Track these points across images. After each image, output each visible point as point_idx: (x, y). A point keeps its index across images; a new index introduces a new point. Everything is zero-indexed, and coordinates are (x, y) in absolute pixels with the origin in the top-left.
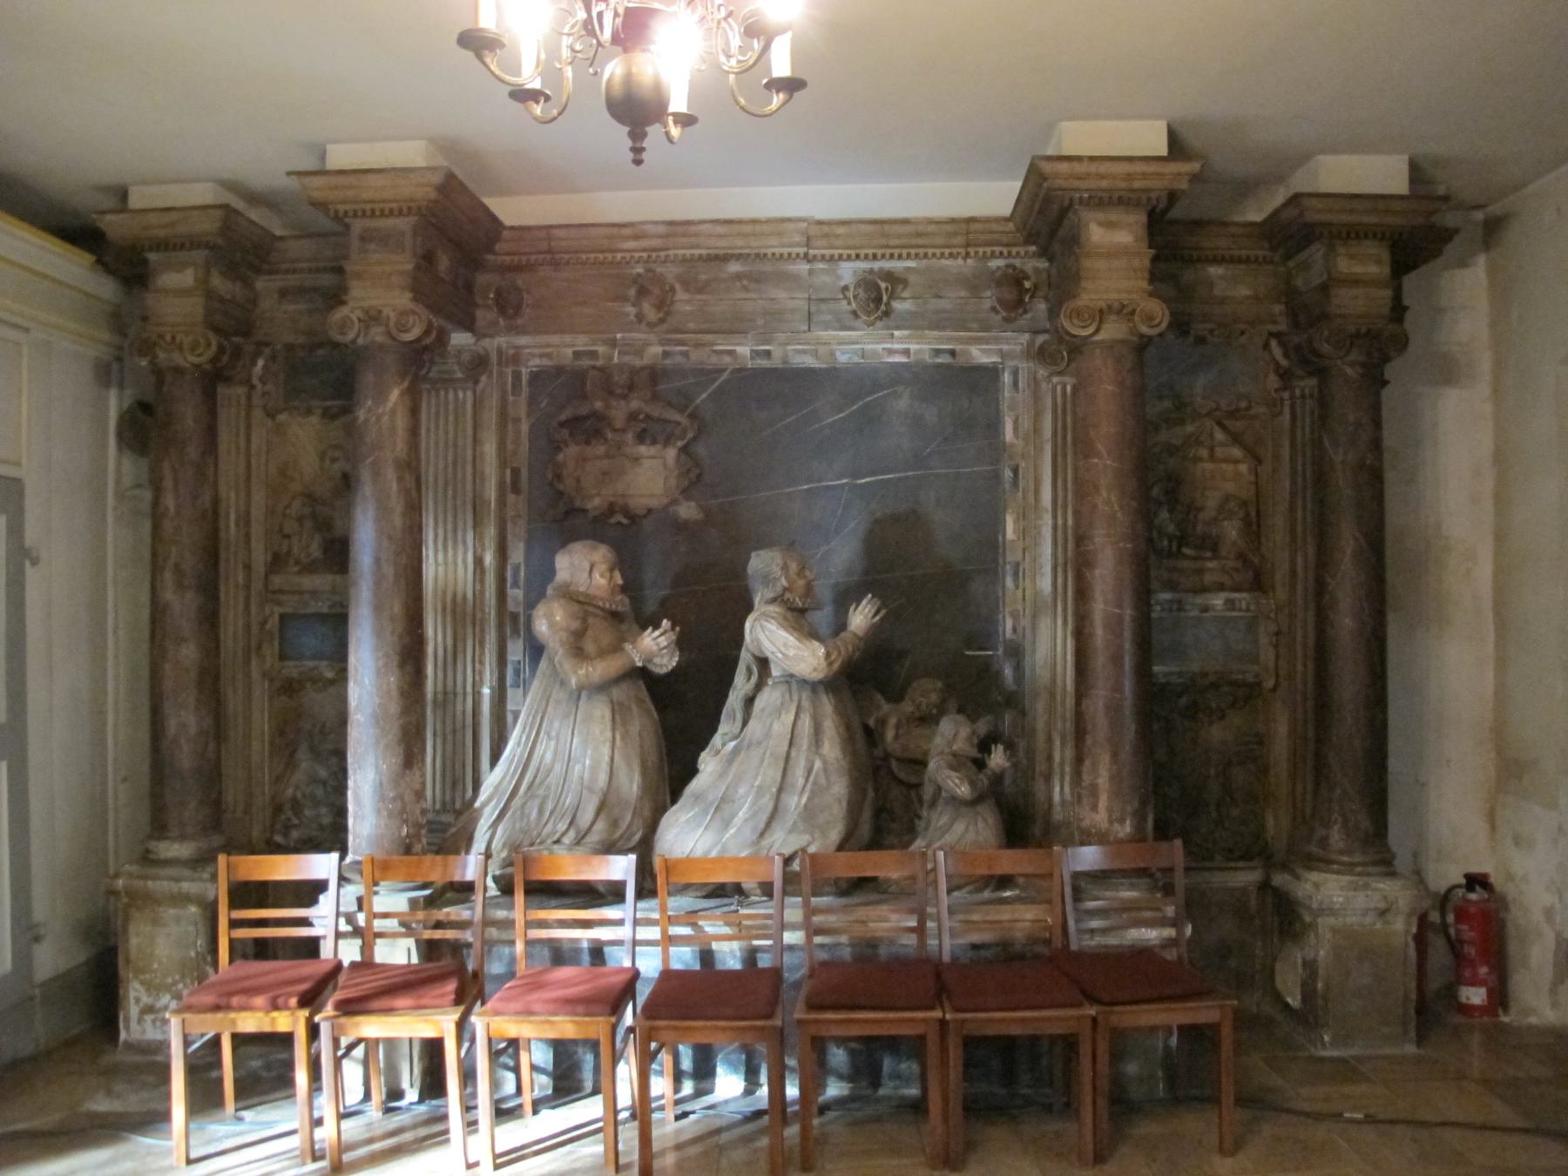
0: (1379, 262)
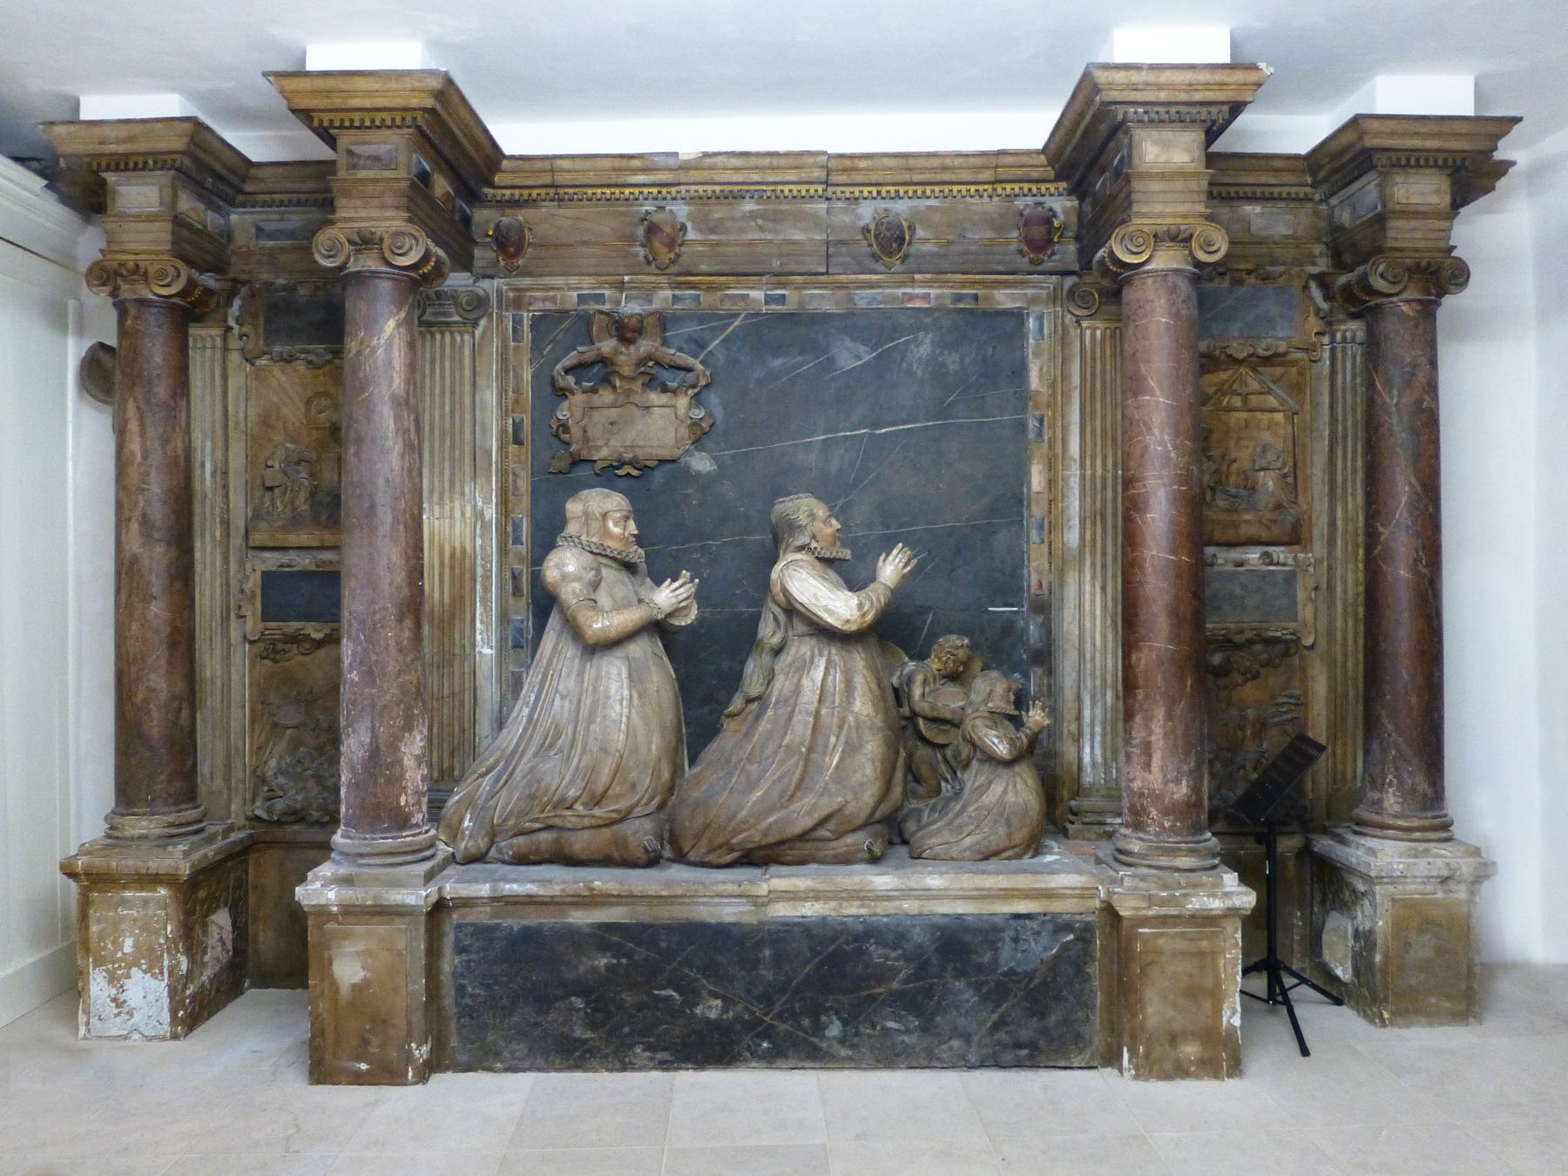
0: (1437, 192)
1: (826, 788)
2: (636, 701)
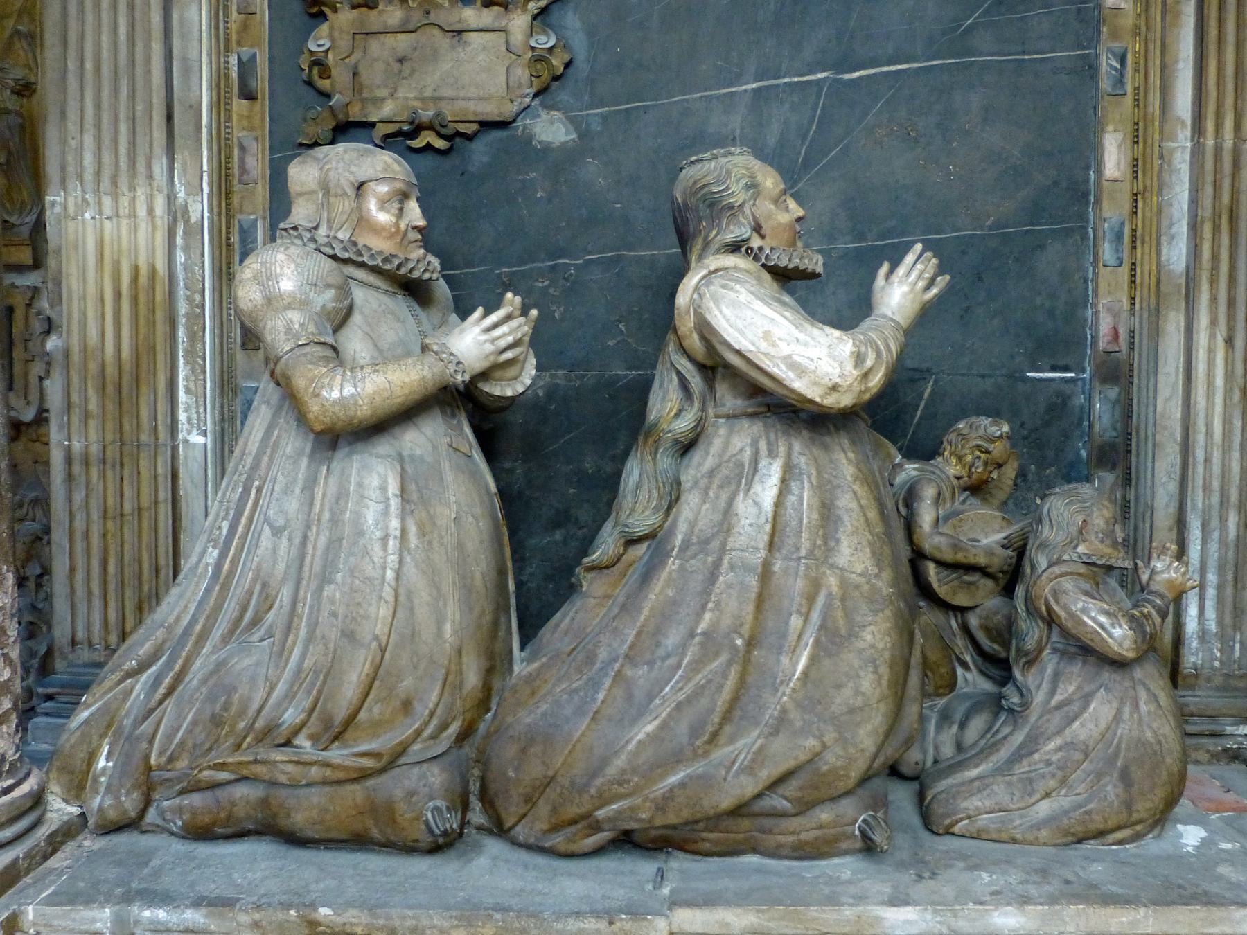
1: (782, 721)
2: (413, 540)
